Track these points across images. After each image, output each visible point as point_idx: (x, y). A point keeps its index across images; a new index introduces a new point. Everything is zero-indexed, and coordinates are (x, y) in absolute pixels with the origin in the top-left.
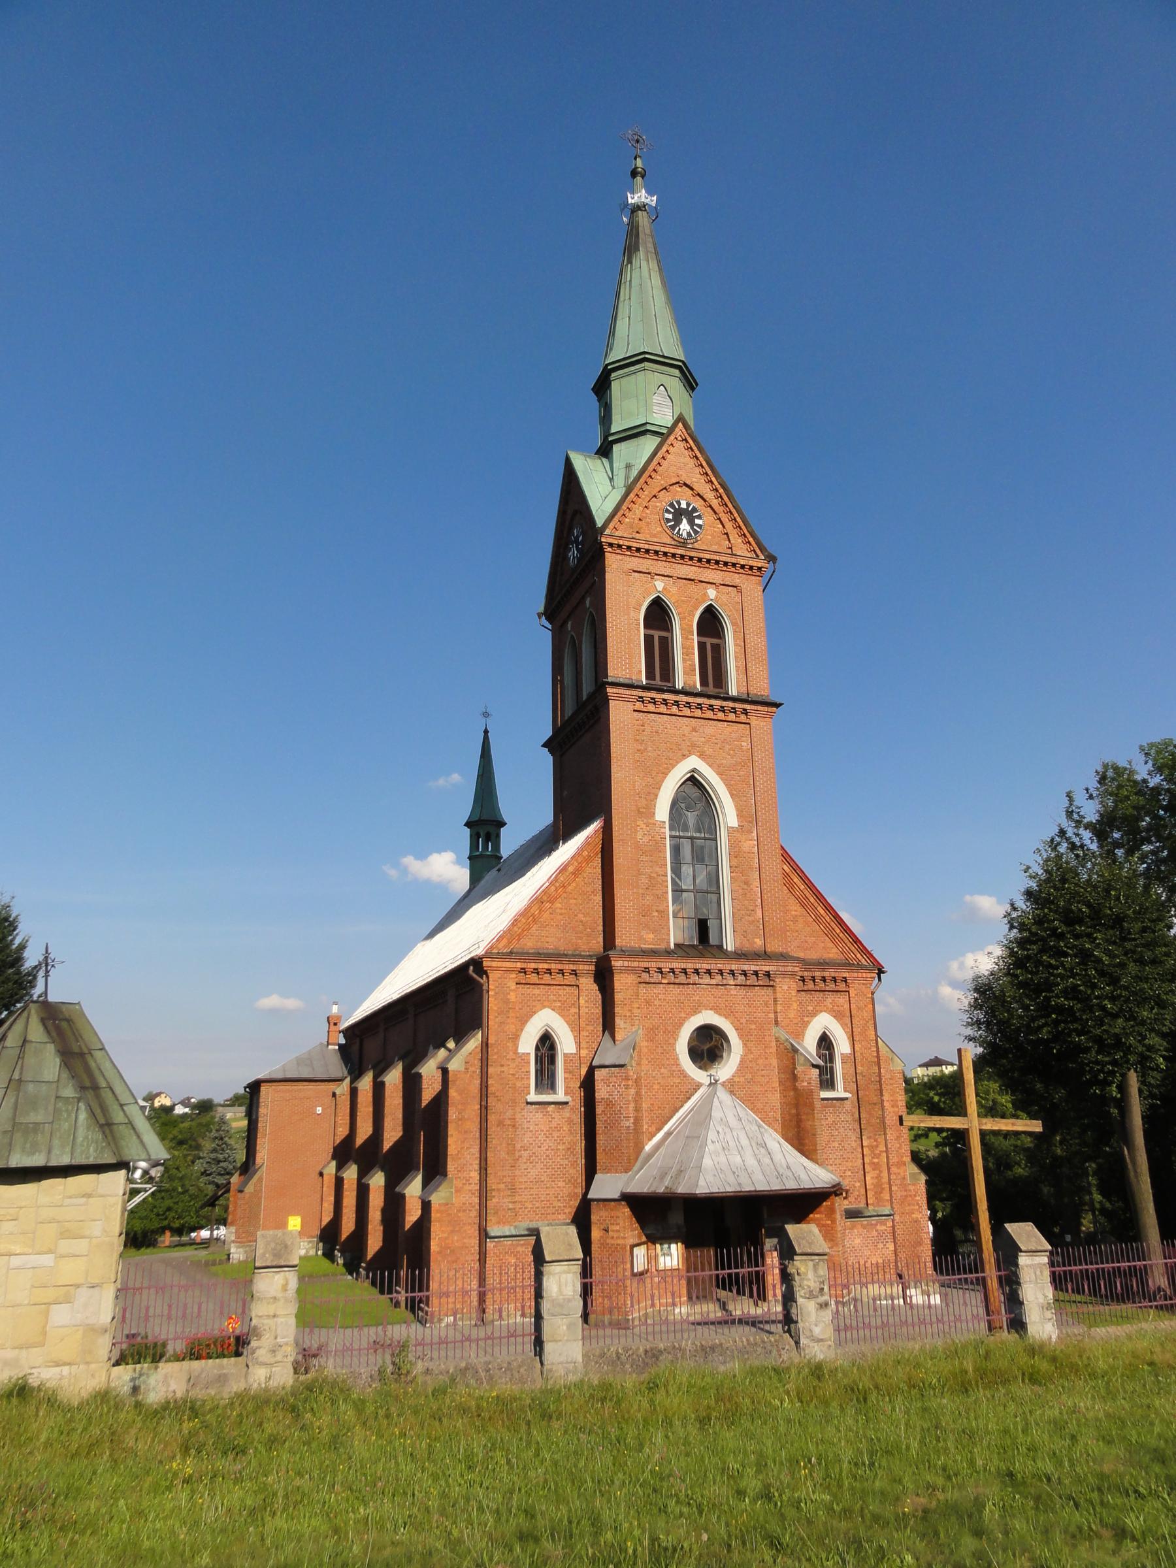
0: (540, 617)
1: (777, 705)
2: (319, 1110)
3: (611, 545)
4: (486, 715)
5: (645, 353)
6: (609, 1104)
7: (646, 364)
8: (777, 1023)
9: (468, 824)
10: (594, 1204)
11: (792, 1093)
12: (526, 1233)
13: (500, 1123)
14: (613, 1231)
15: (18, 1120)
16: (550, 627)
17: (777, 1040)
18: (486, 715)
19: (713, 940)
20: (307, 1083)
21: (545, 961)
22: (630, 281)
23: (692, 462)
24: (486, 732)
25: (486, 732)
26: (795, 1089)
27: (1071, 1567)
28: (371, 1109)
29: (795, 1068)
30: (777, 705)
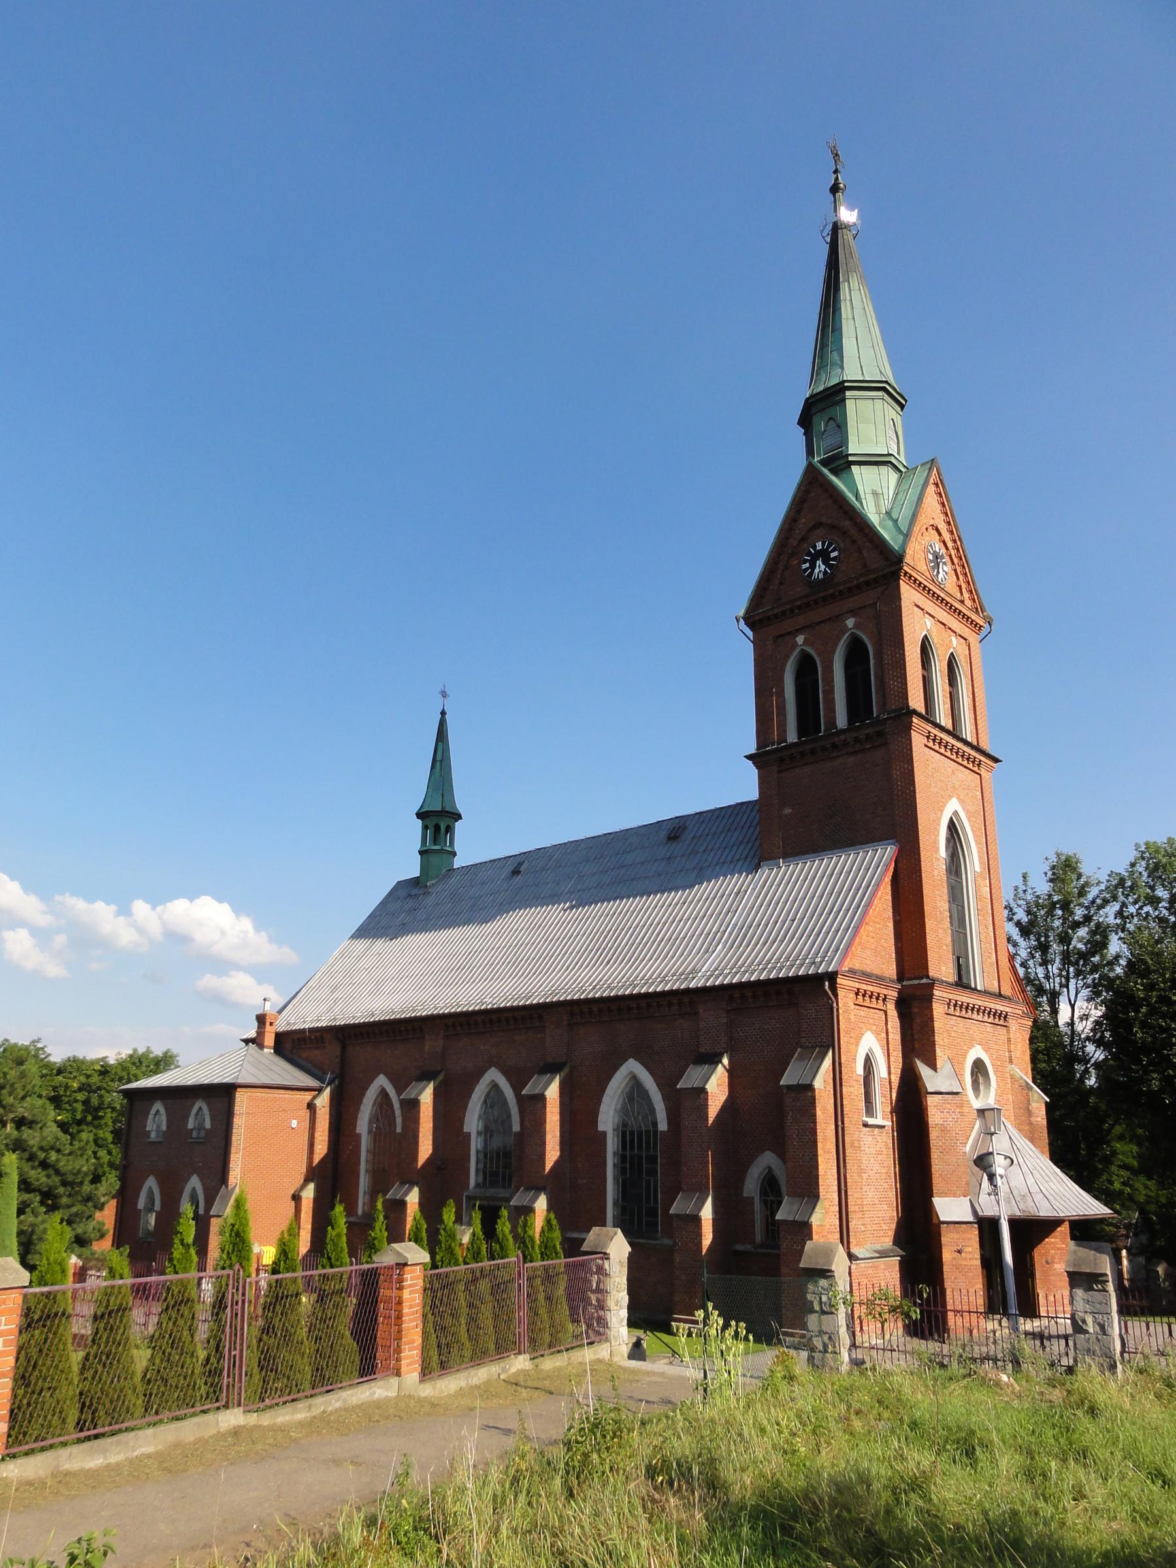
0: (738, 620)
1: (996, 760)
2: (294, 1123)
3: (906, 573)
4: (444, 694)
5: (886, 382)
6: (944, 1129)
7: (880, 393)
8: (1011, 1062)
9: (420, 815)
10: (943, 1227)
11: (1027, 1128)
12: (877, 1255)
13: (852, 1142)
14: (966, 1252)
15: (986, 1113)
16: (750, 634)
17: (1012, 1077)
18: (444, 694)
19: (965, 981)
20: (302, 1093)
21: (871, 984)
22: (851, 300)
23: (939, 507)
24: (443, 713)
25: (443, 713)
26: (1030, 1123)
27: (942, 1564)
28: (431, 1125)
29: (1029, 1104)
30: (996, 760)
